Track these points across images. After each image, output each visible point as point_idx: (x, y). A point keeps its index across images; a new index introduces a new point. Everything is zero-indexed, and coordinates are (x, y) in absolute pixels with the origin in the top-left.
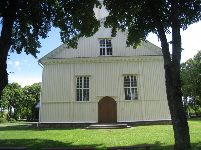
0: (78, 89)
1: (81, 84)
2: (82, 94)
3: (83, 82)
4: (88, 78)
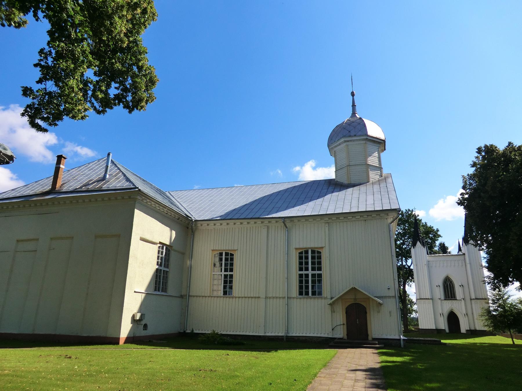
0: (301, 272)
1: (307, 263)
2: (312, 280)
3: (310, 261)
4: (232, 255)
